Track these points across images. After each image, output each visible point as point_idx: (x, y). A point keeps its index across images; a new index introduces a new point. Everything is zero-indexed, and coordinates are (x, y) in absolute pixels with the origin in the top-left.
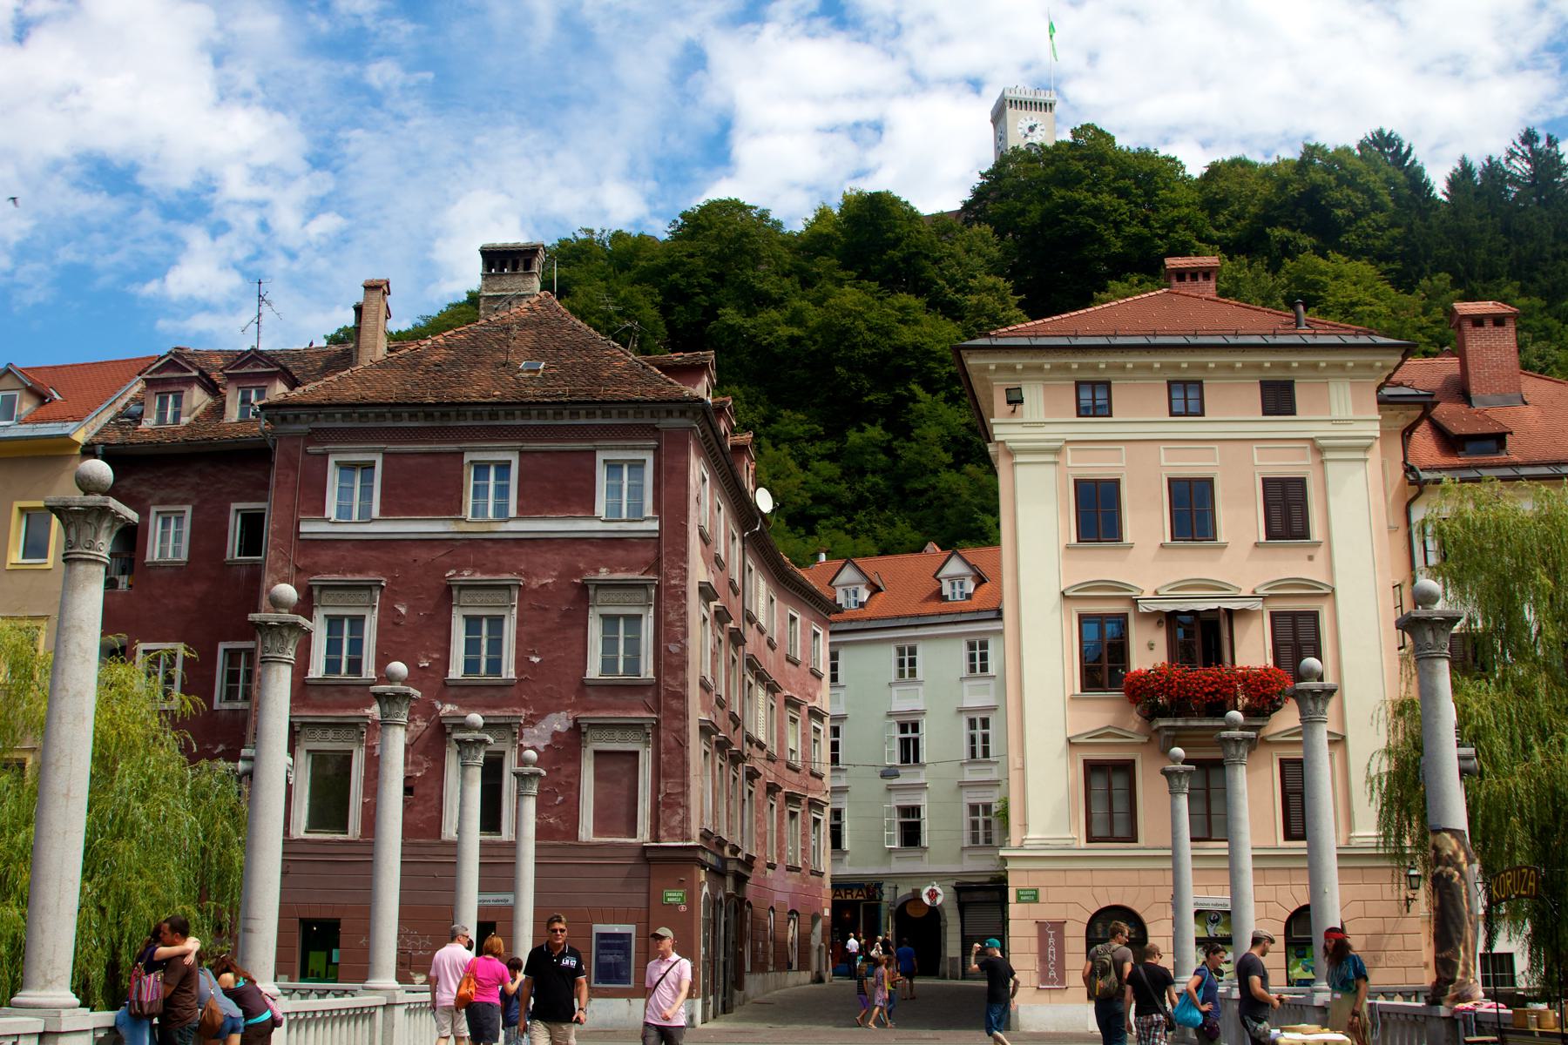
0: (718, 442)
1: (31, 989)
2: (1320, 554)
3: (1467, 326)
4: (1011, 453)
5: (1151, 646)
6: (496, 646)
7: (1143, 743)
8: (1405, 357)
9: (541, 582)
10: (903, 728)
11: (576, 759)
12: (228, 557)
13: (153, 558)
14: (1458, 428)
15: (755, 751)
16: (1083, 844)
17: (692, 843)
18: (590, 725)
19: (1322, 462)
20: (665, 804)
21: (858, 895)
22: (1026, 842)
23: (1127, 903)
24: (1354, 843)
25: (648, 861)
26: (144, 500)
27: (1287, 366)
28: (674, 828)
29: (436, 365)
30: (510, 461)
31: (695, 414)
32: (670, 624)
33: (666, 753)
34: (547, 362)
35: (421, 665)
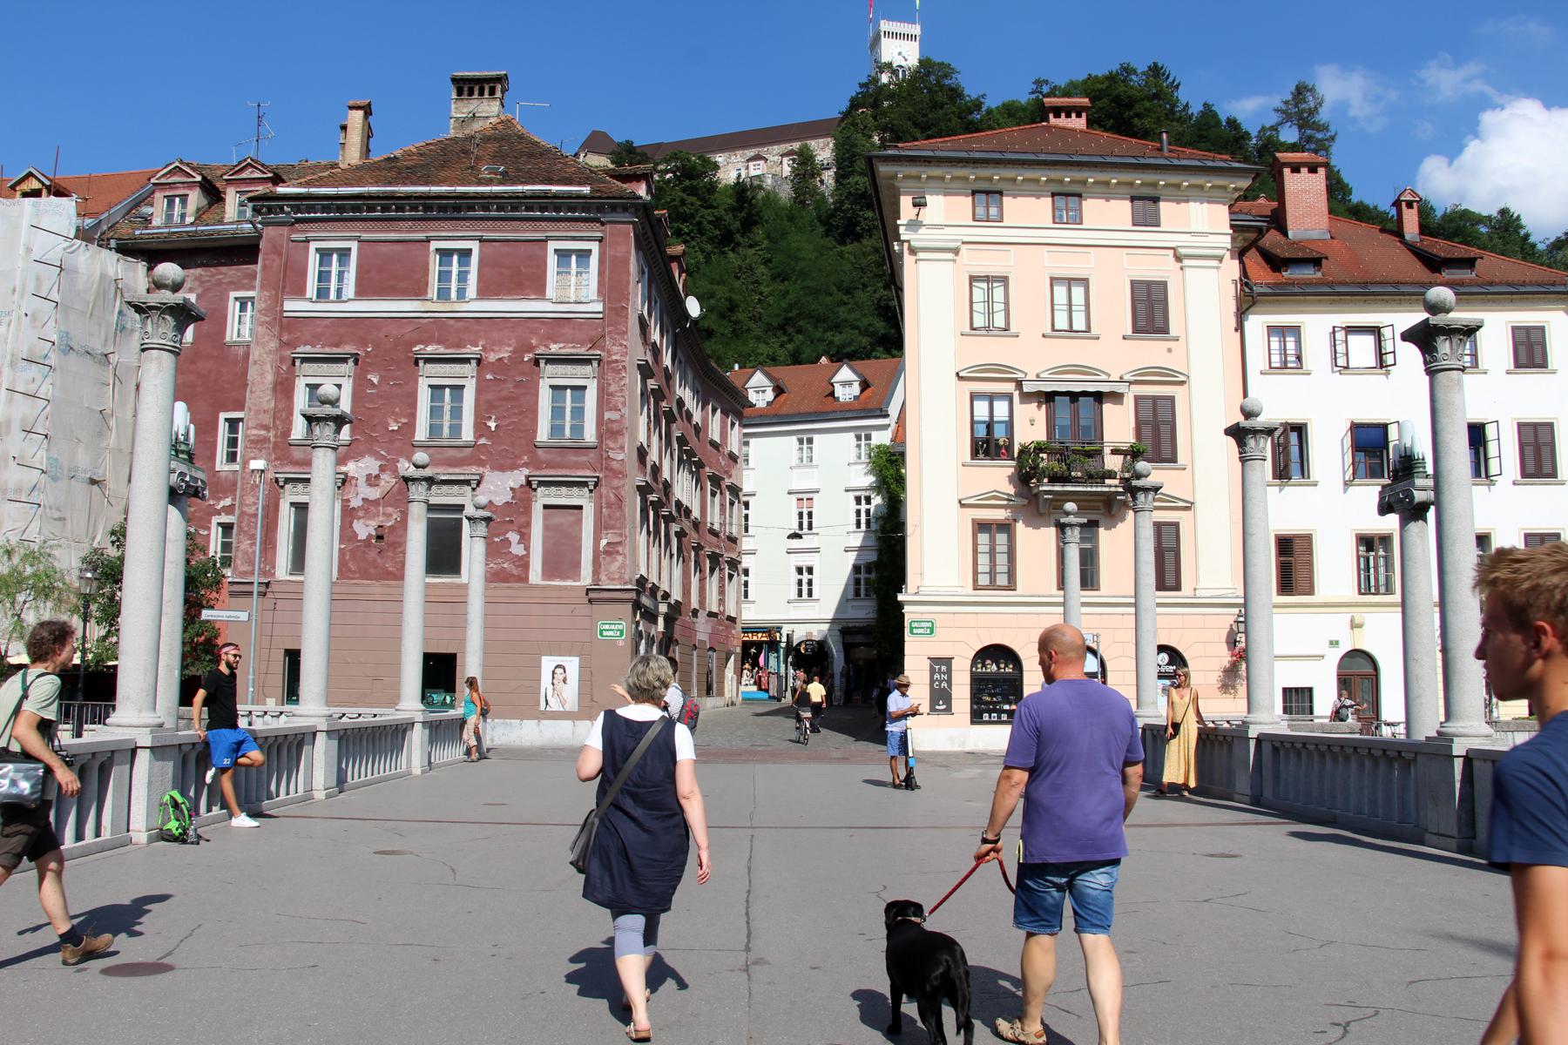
0: (656, 240)
3: (1287, 171)
4: (913, 251)
6: (457, 412)
7: (1024, 506)
9: (497, 357)
11: (527, 511)
16: (970, 590)
17: (629, 587)
18: (539, 482)
24: (1198, 593)
27: (1155, 185)
28: (613, 573)
30: (471, 250)
31: (637, 210)
33: (607, 507)
35: (390, 429)
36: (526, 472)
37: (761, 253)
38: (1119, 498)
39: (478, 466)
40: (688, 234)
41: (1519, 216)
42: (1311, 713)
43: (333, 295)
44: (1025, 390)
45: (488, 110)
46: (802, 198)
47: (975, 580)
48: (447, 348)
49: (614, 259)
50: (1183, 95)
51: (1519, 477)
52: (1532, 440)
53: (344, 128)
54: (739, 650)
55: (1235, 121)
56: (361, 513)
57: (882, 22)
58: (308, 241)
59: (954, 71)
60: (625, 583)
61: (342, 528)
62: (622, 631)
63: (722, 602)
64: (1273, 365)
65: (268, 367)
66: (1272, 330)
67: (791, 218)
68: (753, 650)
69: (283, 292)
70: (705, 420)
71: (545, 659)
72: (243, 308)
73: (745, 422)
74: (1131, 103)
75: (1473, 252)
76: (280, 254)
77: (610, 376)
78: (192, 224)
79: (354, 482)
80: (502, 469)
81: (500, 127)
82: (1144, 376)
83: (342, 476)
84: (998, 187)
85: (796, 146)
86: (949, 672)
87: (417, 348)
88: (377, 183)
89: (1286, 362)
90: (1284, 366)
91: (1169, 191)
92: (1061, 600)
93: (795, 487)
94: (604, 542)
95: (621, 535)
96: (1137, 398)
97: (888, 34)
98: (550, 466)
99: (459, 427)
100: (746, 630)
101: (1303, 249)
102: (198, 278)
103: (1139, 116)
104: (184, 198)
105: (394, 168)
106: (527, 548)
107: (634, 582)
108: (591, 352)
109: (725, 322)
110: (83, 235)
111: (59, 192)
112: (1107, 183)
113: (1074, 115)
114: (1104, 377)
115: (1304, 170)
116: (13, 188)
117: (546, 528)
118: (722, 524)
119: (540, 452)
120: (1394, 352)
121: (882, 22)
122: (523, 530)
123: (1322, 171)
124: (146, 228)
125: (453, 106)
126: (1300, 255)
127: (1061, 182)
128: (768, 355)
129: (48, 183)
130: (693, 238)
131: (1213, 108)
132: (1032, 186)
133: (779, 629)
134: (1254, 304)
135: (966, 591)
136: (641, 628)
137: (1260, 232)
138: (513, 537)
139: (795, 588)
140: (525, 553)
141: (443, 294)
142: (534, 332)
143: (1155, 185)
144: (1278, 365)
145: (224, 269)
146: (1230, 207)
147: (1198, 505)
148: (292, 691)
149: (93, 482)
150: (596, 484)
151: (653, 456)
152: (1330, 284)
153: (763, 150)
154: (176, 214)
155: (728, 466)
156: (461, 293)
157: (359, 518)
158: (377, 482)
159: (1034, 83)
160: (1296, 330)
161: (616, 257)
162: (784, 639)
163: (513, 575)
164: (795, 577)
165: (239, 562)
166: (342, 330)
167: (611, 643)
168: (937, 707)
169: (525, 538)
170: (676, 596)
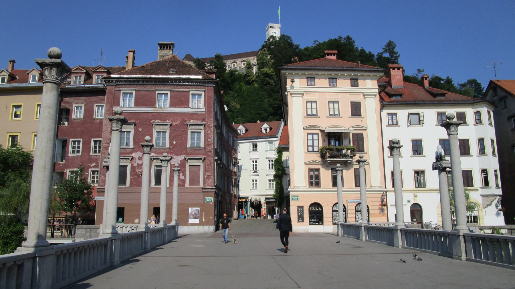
3: (391, 70)
7: (322, 164)
10: (253, 162)
12: (94, 117)
13: (74, 117)
21: (243, 200)
22: (295, 187)
23: (318, 202)
26: (72, 103)
27: (357, 75)
28: (209, 184)
32: (208, 134)
33: (207, 166)
36: (184, 156)
38: (349, 162)
39: (170, 154)
45: (168, 53)
48: (161, 121)
49: (208, 97)
53: (127, 57)
58: (120, 90)
60: (213, 187)
62: (212, 200)
64: (389, 124)
66: (389, 114)
69: (113, 105)
75: (445, 92)
76: (112, 94)
77: (208, 129)
78: (83, 84)
79: (134, 159)
80: (178, 155)
81: (173, 58)
82: (355, 127)
83: (131, 157)
84: (314, 76)
85: (246, 59)
86: (303, 210)
87: (153, 121)
88: (140, 74)
90: (393, 124)
91: (361, 77)
93: (252, 157)
95: (211, 173)
98: (191, 154)
99: (165, 143)
101: (397, 91)
102: (85, 100)
104: (80, 76)
105: (143, 70)
106: (185, 177)
108: (202, 122)
112: (344, 75)
113: (333, 55)
115: (396, 69)
120: (424, 120)
122: (183, 172)
123: (401, 70)
124: (69, 85)
125: (159, 51)
126: (396, 93)
127: (331, 75)
132: (323, 76)
133: (248, 198)
134: (384, 107)
137: (385, 87)
138: (181, 174)
139: (251, 186)
140: (184, 178)
143: (357, 75)
144: (391, 124)
145: (93, 97)
146: (378, 81)
150: (205, 159)
152: (405, 101)
153: (236, 60)
154: (78, 81)
158: (141, 159)
159: (314, 41)
160: (395, 114)
162: (249, 200)
165: (100, 182)
167: (209, 203)
168: (300, 220)
169: (184, 174)
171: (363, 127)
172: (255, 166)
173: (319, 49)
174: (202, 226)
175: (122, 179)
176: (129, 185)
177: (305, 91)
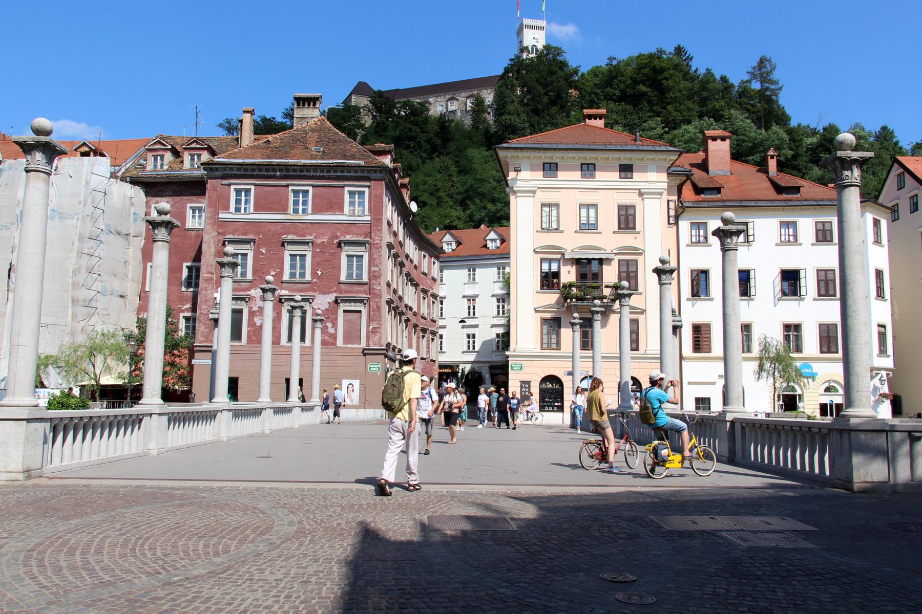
1: (858, 406)
2: (639, 236)
3: (710, 141)
5: (569, 272)
6: (303, 266)
8: (679, 156)
11: (336, 313)
14: (701, 185)
15: (409, 312)
16: (539, 350)
17: (383, 348)
19: (643, 199)
20: (372, 332)
24: (647, 352)
25: (365, 355)
29: (276, 148)
31: (386, 172)
34: (324, 148)
36: (335, 295)
37: (453, 158)
40: (413, 148)
41: (893, 130)
42: (710, 409)
43: (243, 211)
44: (566, 257)
46: (477, 125)
47: (542, 345)
48: (298, 236)
49: (376, 195)
50: (694, 65)
51: (817, 296)
52: (824, 278)
54: (437, 377)
55: (725, 77)
56: (258, 314)
57: (524, 19)
59: (563, 52)
60: (381, 346)
61: (249, 320)
62: (379, 368)
63: (428, 352)
65: (212, 244)
67: (470, 138)
68: (444, 377)
70: (420, 262)
71: (344, 381)
72: (194, 212)
73: (441, 260)
74: (662, 70)
76: (216, 190)
78: (167, 170)
79: (254, 299)
80: (324, 293)
89: (699, 240)
90: (699, 242)
92: (592, 355)
94: (371, 327)
96: (619, 261)
97: (527, 26)
98: (346, 292)
100: (441, 367)
103: (666, 79)
104: (162, 157)
106: (336, 330)
107: (385, 345)
109: (433, 198)
110: (113, 175)
111: (98, 153)
114: (603, 251)
116: (76, 150)
117: (345, 321)
118: (429, 314)
119: (341, 285)
121: (524, 19)
128: (456, 216)
129: (94, 148)
130: (416, 150)
131: (712, 71)
133: (458, 366)
135: (537, 350)
136: (388, 366)
138: (329, 325)
140: (334, 332)
141: (296, 211)
142: (339, 229)
147: (647, 310)
148: (212, 396)
149: (122, 296)
151: (394, 286)
155: (432, 284)
156: (304, 211)
157: (257, 316)
159: (608, 59)
161: (376, 195)
162: (460, 371)
163: (329, 342)
164: (466, 340)
166: (247, 228)
169: (335, 325)
170: (415, 309)
171: (637, 249)
172: (501, 307)
173: (616, 77)
174: (363, 410)
175: (236, 334)
176: (246, 342)
177: (539, 186)
